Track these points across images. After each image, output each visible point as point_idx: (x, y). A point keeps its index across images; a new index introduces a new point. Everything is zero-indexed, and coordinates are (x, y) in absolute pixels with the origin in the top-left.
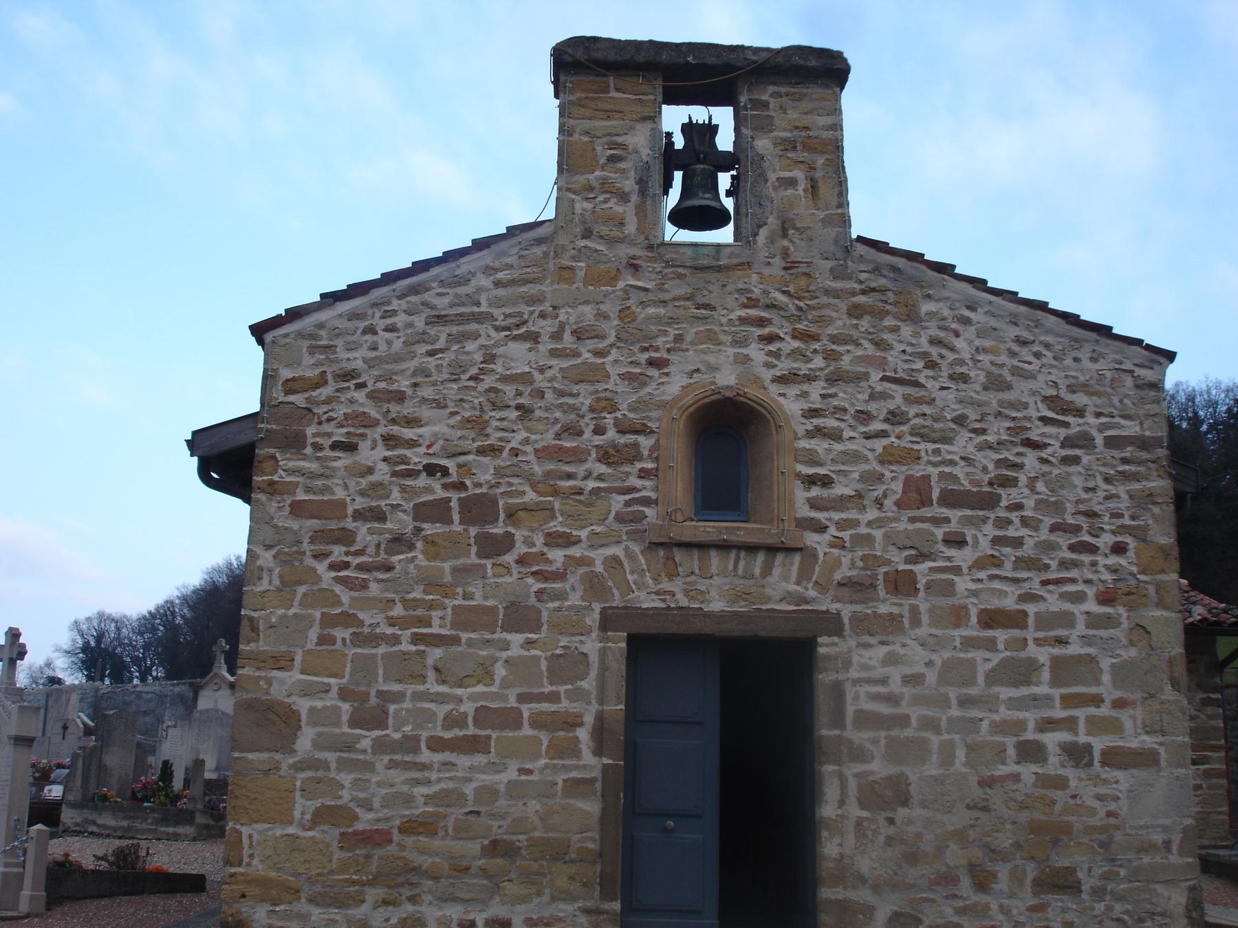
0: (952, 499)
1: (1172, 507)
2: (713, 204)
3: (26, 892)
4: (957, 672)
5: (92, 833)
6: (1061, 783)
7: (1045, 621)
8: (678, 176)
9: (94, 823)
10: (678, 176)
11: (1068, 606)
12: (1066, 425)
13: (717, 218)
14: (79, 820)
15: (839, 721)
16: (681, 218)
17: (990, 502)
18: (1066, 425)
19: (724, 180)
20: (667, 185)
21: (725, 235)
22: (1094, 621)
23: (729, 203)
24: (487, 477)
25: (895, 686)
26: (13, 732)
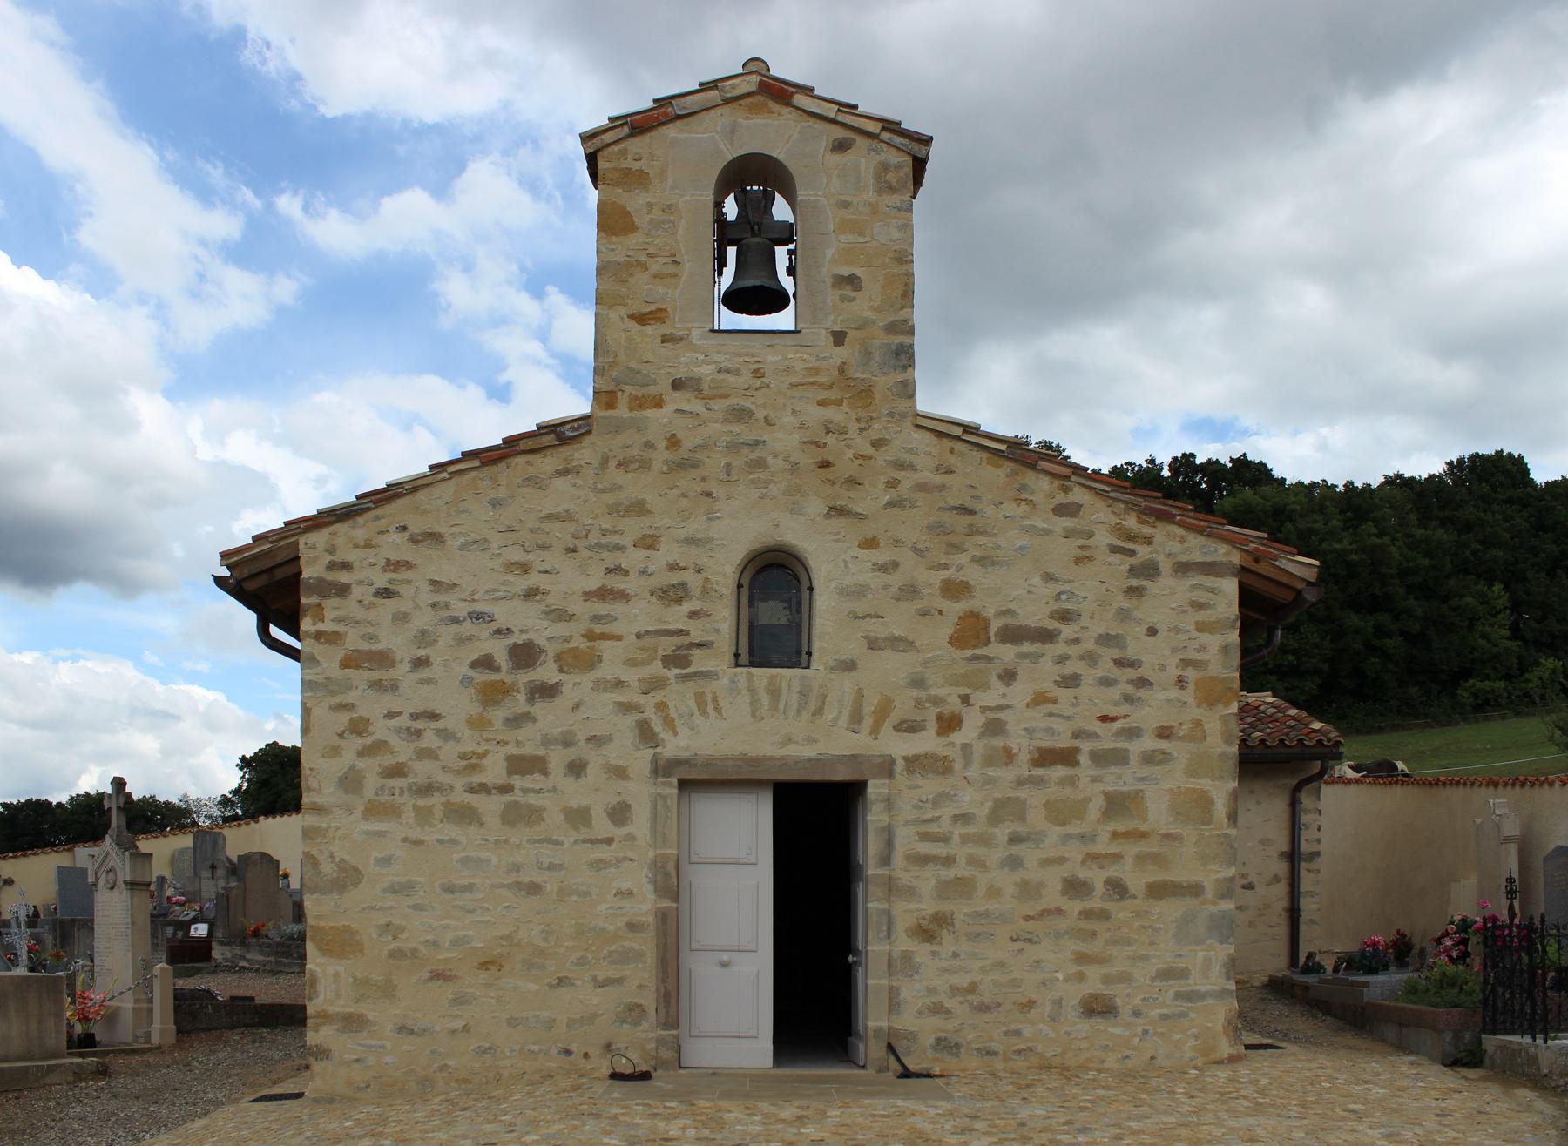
0: (1013, 635)
1: (1234, 637)
2: (766, 283)
3: (156, 1025)
4: (1003, 809)
5: (243, 968)
6: (1104, 915)
7: (1099, 758)
8: (732, 252)
9: (243, 958)
10: (732, 252)
11: (1122, 744)
12: (1132, 553)
13: (773, 300)
14: (229, 955)
15: (886, 860)
16: (738, 300)
17: (1047, 636)
18: (1132, 553)
19: (781, 254)
20: (722, 262)
21: (783, 320)
22: (1149, 758)
23: (787, 283)
24: (970, 1037)
25: (945, 825)
26: (128, 879)
